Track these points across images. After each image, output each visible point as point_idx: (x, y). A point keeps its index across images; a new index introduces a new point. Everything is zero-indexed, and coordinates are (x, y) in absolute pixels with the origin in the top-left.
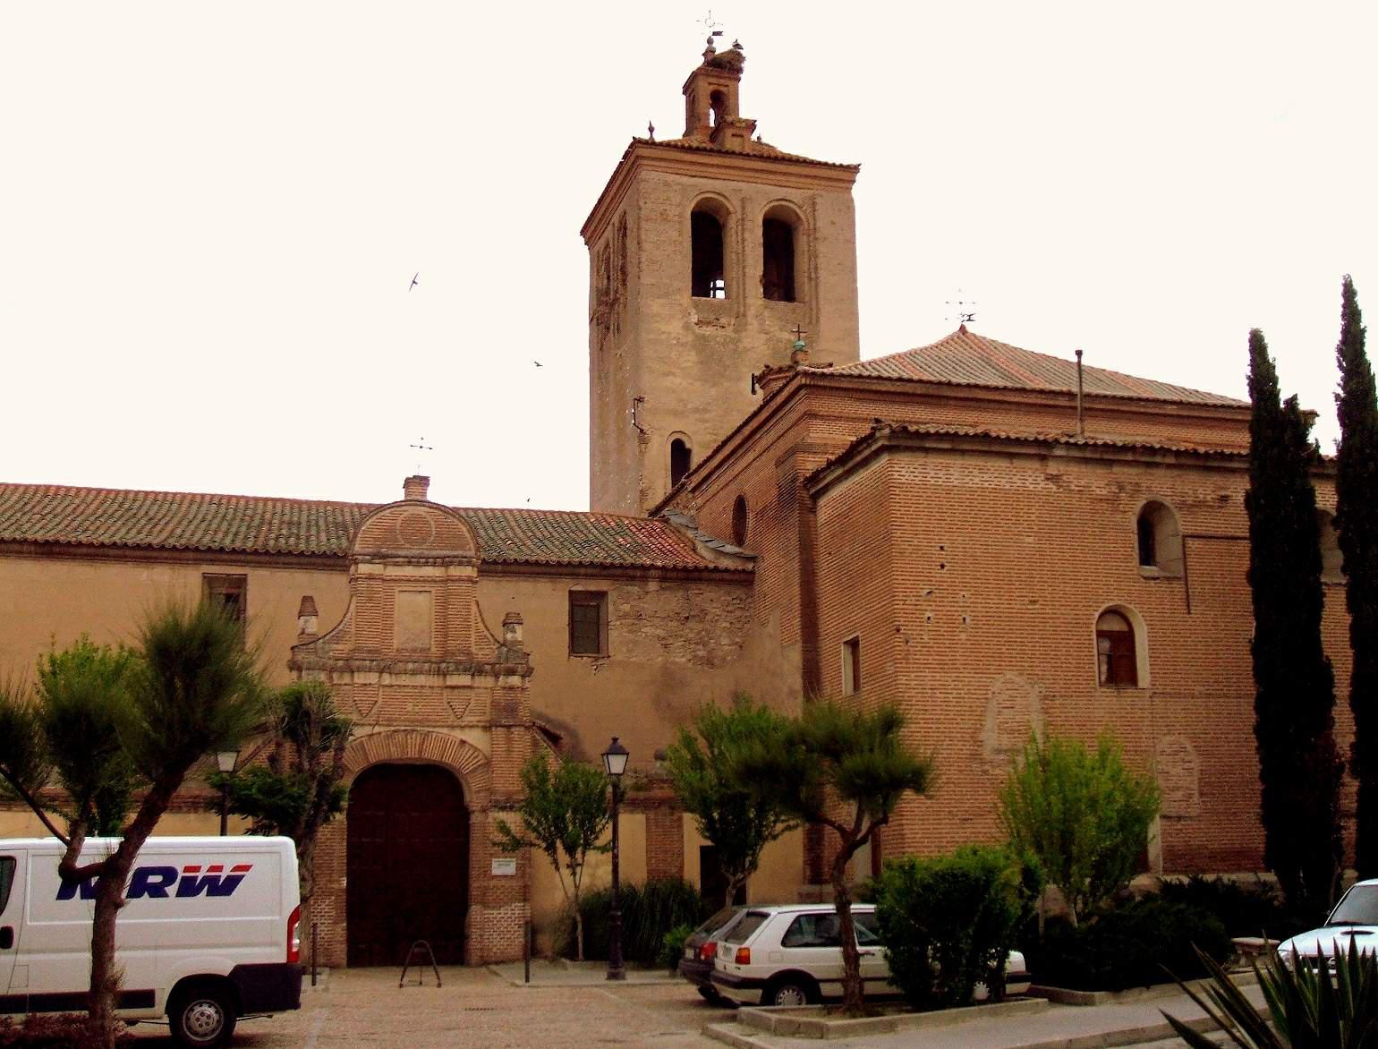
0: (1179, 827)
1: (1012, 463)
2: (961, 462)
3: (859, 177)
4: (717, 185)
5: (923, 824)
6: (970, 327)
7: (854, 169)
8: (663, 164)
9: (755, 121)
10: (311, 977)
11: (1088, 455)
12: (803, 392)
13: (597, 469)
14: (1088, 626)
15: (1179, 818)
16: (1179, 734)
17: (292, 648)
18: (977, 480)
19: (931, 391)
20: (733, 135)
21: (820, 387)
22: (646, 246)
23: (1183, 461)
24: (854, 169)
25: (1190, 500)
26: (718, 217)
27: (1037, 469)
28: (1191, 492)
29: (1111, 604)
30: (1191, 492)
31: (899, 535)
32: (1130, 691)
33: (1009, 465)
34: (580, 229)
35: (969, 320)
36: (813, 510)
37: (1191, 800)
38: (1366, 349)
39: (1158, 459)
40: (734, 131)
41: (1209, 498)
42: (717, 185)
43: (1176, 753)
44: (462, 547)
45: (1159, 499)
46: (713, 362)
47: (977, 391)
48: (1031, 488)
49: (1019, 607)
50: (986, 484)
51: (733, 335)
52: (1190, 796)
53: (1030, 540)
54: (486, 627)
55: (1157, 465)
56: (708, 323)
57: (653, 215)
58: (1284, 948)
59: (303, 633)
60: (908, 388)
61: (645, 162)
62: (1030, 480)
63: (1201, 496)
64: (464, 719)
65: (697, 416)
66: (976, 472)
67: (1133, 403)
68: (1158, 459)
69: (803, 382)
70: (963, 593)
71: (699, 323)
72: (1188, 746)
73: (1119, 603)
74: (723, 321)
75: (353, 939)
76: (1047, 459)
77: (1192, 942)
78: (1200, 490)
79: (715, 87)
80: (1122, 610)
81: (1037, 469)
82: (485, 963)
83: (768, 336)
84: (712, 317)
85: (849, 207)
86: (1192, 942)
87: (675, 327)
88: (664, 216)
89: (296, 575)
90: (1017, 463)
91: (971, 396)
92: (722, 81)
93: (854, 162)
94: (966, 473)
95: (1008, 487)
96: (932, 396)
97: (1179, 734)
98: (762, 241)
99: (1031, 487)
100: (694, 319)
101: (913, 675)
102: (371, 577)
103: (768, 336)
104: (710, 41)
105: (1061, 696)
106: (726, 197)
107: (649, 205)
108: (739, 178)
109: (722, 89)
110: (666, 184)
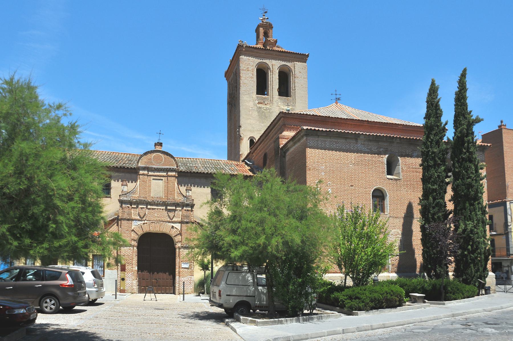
0: (396, 258)
1: (346, 141)
3: (309, 59)
9: (277, 40)
10: (182, 295)
12: (282, 119)
13: (229, 148)
14: (369, 194)
17: (120, 195)
18: (334, 146)
21: (287, 117)
24: (308, 56)
26: (265, 70)
27: (354, 143)
29: (376, 187)
31: (309, 163)
33: (345, 141)
36: (284, 157)
41: (410, 153)
44: (172, 165)
46: (262, 114)
48: (352, 149)
49: (347, 187)
50: (337, 147)
53: (351, 166)
54: (180, 191)
56: (261, 103)
59: (123, 191)
64: (174, 219)
65: (258, 132)
66: (334, 143)
69: (282, 116)
70: (329, 182)
71: (259, 103)
73: (380, 187)
74: (266, 103)
75: (140, 285)
77: (425, 295)
78: (407, 151)
83: (280, 108)
84: (262, 101)
86: (425, 295)
87: (251, 104)
89: (132, 175)
94: (331, 144)
99: (352, 149)
100: (257, 102)
102: (143, 175)
103: (280, 108)
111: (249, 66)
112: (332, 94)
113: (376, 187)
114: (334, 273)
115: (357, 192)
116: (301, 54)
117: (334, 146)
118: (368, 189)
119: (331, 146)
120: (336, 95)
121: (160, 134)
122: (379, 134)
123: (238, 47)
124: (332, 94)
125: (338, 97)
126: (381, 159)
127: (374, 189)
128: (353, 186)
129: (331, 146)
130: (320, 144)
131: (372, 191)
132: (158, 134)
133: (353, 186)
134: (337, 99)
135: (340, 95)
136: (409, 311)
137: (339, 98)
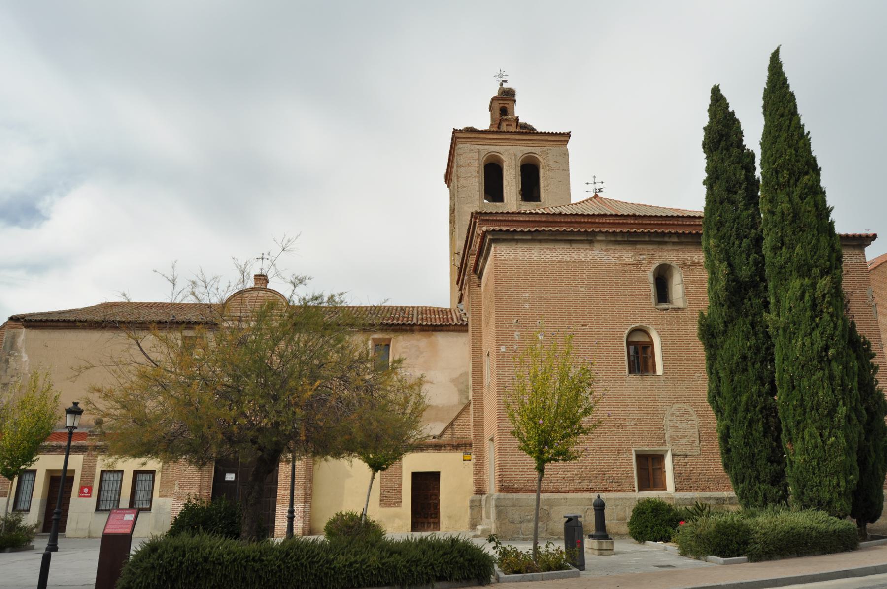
2: (539, 246)
4: (497, 148)
5: (511, 458)
6: (600, 195)
7: (568, 135)
8: (468, 140)
11: (619, 239)
14: (621, 338)
15: (686, 456)
16: (684, 403)
18: (548, 256)
19: (550, 219)
20: (507, 125)
22: (461, 179)
23: (683, 240)
24: (568, 135)
25: (689, 263)
28: (689, 258)
30: (689, 258)
32: (650, 377)
34: (444, 180)
35: (599, 192)
37: (694, 444)
38: (709, 102)
39: (666, 239)
40: (508, 123)
42: (497, 148)
43: (683, 415)
45: (667, 262)
47: (577, 217)
51: (774, 318)
52: (693, 442)
53: (583, 289)
55: (665, 243)
57: (464, 164)
58: (137, 536)
60: (537, 218)
61: (460, 140)
62: (583, 255)
63: (697, 260)
67: (674, 219)
68: (666, 239)
70: (539, 321)
72: (690, 410)
73: (642, 324)
76: (594, 242)
79: (501, 105)
80: (645, 329)
81: (587, 249)
82: (874, 538)
85: (566, 154)
88: (469, 165)
90: (574, 245)
91: (574, 220)
92: (505, 102)
93: (566, 131)
94: (542, 253)
95: (568, 259)
96: (551, 222)
97: (684, 403)
98: (520, 173)
99: (583, 259)
101: (506, 368)
104: (501, 85)
105: (603, 381)
106: (500, 153)
107: (462, 160)
108: (501, 144)
109: (506, 106)
110: (471, 149)
111: (472, 161)
112: (587, 183)
113: (633, 326)
114: (552, 492)
115: (596, 336)
116: (556, 133)
117: (548, 256)
118: (618, 330)
119: (542, 256)
120: (595, 183)
121: (263, 259)
122: (635, 230)
123: (454, 133)
124: (587, 183)
125: (598, 186)
126: (643, 273)
127: (629, 329)
128: (586, 325)
129: (542, 256)
130: (521, 254)
131: (627, 332)
132: (260, 260)
133: (586, 325)
134: (598, 190)
135: (602, 183)
136: (564, 573)
137: (600, 189)
